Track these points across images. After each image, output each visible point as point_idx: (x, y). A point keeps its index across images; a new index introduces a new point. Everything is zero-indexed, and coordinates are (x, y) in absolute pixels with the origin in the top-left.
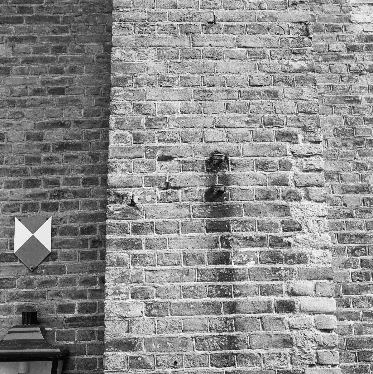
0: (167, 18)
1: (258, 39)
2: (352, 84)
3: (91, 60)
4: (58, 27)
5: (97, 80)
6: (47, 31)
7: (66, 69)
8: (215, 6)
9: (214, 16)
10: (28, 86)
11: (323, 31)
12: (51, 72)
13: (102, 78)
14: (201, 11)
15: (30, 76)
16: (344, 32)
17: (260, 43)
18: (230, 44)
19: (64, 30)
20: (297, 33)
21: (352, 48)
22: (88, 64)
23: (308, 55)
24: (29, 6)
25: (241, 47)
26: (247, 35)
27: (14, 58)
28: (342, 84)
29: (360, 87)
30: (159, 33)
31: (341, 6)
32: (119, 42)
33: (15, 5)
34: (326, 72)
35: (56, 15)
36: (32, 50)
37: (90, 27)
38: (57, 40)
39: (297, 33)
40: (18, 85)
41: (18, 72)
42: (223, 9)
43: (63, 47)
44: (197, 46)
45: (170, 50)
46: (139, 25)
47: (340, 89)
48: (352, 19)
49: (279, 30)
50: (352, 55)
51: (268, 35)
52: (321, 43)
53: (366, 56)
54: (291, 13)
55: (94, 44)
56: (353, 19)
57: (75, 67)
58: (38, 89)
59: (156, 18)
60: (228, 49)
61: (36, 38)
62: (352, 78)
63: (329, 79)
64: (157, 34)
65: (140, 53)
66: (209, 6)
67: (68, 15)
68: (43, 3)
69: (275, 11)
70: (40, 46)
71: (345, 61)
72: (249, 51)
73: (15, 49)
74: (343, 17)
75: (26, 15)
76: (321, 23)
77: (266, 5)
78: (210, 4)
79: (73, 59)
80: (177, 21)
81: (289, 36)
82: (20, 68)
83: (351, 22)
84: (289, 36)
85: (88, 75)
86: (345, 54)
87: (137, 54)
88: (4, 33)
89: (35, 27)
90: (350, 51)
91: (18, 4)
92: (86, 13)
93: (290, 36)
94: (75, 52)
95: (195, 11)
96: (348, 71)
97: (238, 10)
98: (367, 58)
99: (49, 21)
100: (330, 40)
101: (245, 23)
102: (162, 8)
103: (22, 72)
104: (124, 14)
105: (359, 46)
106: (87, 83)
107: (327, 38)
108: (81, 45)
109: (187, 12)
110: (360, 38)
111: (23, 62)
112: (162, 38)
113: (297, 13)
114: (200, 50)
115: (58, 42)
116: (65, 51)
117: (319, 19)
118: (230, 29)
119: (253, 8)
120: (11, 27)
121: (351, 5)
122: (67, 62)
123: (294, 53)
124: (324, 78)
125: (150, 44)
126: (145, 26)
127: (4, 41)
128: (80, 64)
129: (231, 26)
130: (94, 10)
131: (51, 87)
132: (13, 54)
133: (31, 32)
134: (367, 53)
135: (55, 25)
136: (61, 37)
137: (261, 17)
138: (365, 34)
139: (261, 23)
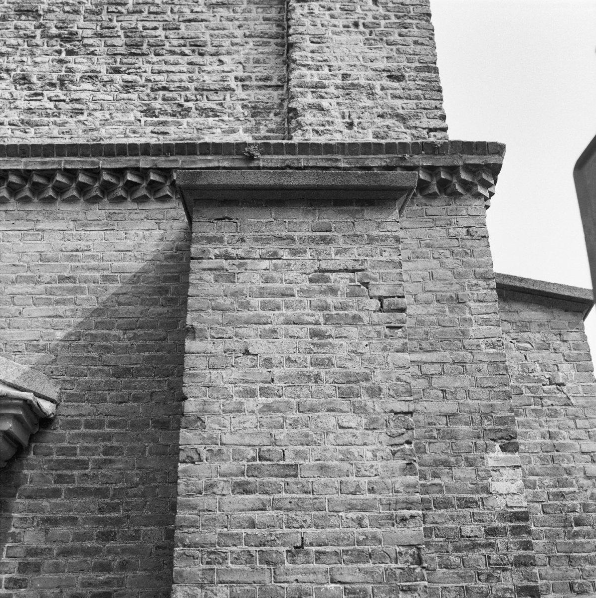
0: (243, 541)
1: (358, 571)
2: (493, 584)
3: (149, 552)
4: (107, 504)
5: (155, 582)
6: (92, 509)
7: (115, 564)
8: (303, 524)
9: (302, 538)
10: (64, 589)
11: (453, 507)
12: (94, 569)
13: (161, 577)
14: (286, 530)
15: (66, 575)
16: (481, 508)
17: (360, 577)
18: (320, 577)
19: (114, 508)
20: (407, 562)
21: (492, 532)
22: (143, 558)
23: (421, 593)
24: (68, 473)
25: (335, 583)
26: (343, 565)
27: (47, 548)
28: (480, 584)
29: (504, 589)
30: (232, 563)
31: (477, 471)
32: (181, 576)
33: (51, 472)
34: (458, 566)
35: (105, 486)
36: (71, 538)
37: (148, 503)
38: (104, 522)
39: (407, 562)
40: (50, 588)
41: (52, 569)
42: (313, 528)
43: (111, 532)
44: (280, 582)
45: (246, 588)
46: (208, 552)
47: (477, 592)
48: (492, 490)
49: (384, 557)
50: (492, 541)
51: (369, 565)
52: (452, 525)
53: (511, 543)
54: (398, 533)
55: (153, 528)
56: (493, 489)
57: (127, 562)
58: (77, 593)
59: (230, 542)
60: (319, 586)
61: (77, 518)
62: (492, 576)
63: (461, 577)
64: (230, 565)
65: (208, 592)
66: (296, 525)
67: (120, 485)
68: (87, 468)
69: (379, 530)
70: (82, 531)
71: (483, 551)
72: (345, 588)
73: (49, 535)
74: (480, 486)
75: (66, 486)
76: (450, 495)
77: (368, 522)
78: (297, 521)
79: (124, 550)
80: (256, 546)
81: (396, 566)
82: (55, 563)
83: (491, 493)
84: (396, 566)
85: (144, 573)
86: (482, 540)
87: (203, 594)
88: (36, 512)
89: (77, 503)
90: (489, 537)
91: (56, 470)
92: (144, 484)
93: (398, 566)
94: (127, 540)
95: (279, 531)
96: (486, 566)
97: (333, 530)
98: (512, 546)
99: (95, 495)
100: (463, 520)
101: (341, 548)
102: (236, 528)
103: (57, 569)
104: (190, 536)
105: (500, 528)
106: (141, 586)
107: (458, 517)
108: (135, 530)
109: (267, 533)
110: (502, 516)
111: (58, 555)
112: (236, 570)
113: (407, 532)
114: (283, 588)
115: (105, 525)
116: (114, 538)
117: (449, 489)
118: (322, 556)
119: (351, 525)
120: (45, 503)
121: (490, 469)
122: (116, 554)
123: (402, 590)
124: (456, 576)
125: (221, 579)
126: (214, 553)
127: (35, 524)
128: (132, 558)
129: (324, 553)
130: (154, 480)
131: (95, 591)
132: (45, 542)
133: (71, 510)
134: (512, 538)
135: (102, 500)
136: (109, 518)
137: (361, 538)
138: (509, 510)
139: (361, 548)
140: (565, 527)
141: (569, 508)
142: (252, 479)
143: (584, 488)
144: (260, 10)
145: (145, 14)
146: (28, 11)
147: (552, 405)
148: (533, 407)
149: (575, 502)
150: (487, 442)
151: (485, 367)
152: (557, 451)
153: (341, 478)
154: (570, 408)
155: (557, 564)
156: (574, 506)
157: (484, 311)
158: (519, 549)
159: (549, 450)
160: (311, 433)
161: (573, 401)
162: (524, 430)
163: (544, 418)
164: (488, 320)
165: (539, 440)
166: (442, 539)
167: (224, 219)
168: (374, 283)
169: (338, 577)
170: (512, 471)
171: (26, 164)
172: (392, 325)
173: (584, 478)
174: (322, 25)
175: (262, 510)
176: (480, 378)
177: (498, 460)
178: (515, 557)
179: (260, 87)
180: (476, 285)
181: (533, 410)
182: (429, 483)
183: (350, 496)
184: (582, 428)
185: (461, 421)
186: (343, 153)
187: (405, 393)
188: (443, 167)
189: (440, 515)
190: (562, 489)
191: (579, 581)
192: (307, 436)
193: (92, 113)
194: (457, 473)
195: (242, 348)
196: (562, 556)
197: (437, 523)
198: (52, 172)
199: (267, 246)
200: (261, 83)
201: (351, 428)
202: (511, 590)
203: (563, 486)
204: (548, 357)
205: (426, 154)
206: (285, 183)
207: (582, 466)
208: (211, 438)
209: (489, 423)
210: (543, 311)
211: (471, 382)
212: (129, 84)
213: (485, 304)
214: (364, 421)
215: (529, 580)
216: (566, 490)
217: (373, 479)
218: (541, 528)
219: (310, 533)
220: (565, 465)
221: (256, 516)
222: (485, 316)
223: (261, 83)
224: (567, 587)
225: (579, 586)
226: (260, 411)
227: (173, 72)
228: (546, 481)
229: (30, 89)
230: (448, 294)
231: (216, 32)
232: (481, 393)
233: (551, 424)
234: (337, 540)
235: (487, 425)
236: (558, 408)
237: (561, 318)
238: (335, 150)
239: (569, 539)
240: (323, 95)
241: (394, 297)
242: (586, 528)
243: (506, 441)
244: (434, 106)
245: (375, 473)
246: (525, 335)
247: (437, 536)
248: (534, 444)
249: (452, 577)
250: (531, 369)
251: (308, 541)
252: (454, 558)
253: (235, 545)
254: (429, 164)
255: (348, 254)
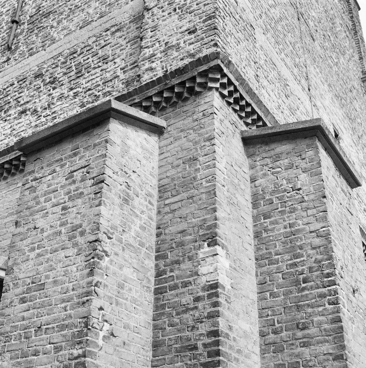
21: (197, 299)
34: (177, 324)
47: (185, 339)
50: (197, 305)
52: (176, 299)
63: (179, 331)
71: (191, 313)
83: (199, 275)
107: (181, 294)
124: (176, 330)
134: (208, 301)
140: (296, 285)
141: (299, 272)
142: (27, 295)
143: (311, 256)
144: (134, 25)
145: (85, 52)
146: (39, 75)
147: (292, 205)
148: (280, 209)
149: (304, 267)
150: (200, 243)
151: (204, 196)
152: (294, 235)
153: (62, 286)
154: (304, 204)
155: (289, 312)
156: (303, 270)
157: (207, 160)
158: (210, 308)
159: (288, 235)
160: (53, 264)
161: (306, 198)
162: (273, 226)
163: (287, 215)
164: (209, 165)
165: (282, 231)
166: (171, 309)
167: (37, 160)
168: (92, 170)
169: (52, 341)
170: (211, 258)
171: (10, 157)
172: (96, 192)
173: (311, 249)
174: (157, 19)
175: (28, 310)
176: (200, 204)
177: (205, 253)
178: (208, 313)
179: (131, 69)
180: (204, 146)
181: (279, 212)
182: (167, 277)
183: (64, 295)
184: (311, 215)
185: (188, 233)
186: (137, 94)
187: (96, 229)
188: (187, 80)
189: (171, 295)
190: (296, 260)
191: (303, 321)
192: (51, 266)
193: (60, 116)
194: (183, 266)
195: (33, 226)
196: (292, 306)
197: (169, 300)
198: (19, 157)
199: (51, 167)
200: (132, 66)
201: (70, 256)
202: (204, 334)
203: (297, 258)
204: (291, 173)
205: (178, 76)
206: (55, 131)
207: (309, 242)
208: (15, 277)
209: (202, 231)
210: (290, 143)
211: (195, 208)
212: (76, 94)
213: (208, 156)
214: (76, 250)
215: (214, 326)
216: (298, 260)
217: (74, 283)
218: (280, 290)
219: (44, 319)
220: (298, 244)
221: (26, 314)
222: (207, 164)
223: (132, 66)
224: (295, 326)
225: (302, 325)
226: (36, 258)
227: (93, 79)
228: (286, 257)
229: (37, 115)
230: (189, 157)
231: (114, 47)
232: (200, 213)
233: (291, 218)
234: (55, 320)
235: (201, 232)
236: (296, 206)
237: (302, 144)
238: (133, 94)
239: (298, 293)
240: (153, 60)
241: (99, 175)
242: (310, 284)
243: (211, 240)
244: (210, 40)
245: (76, 279)
246: (278, 163)
247: (168, 308)
248: (279, 234)
249: (174, 331)
250: (279, 185)
251: (43, 324)
252: (176, 320)
253: (15, 331)
254: (180, 81)
255: (84, 158)
